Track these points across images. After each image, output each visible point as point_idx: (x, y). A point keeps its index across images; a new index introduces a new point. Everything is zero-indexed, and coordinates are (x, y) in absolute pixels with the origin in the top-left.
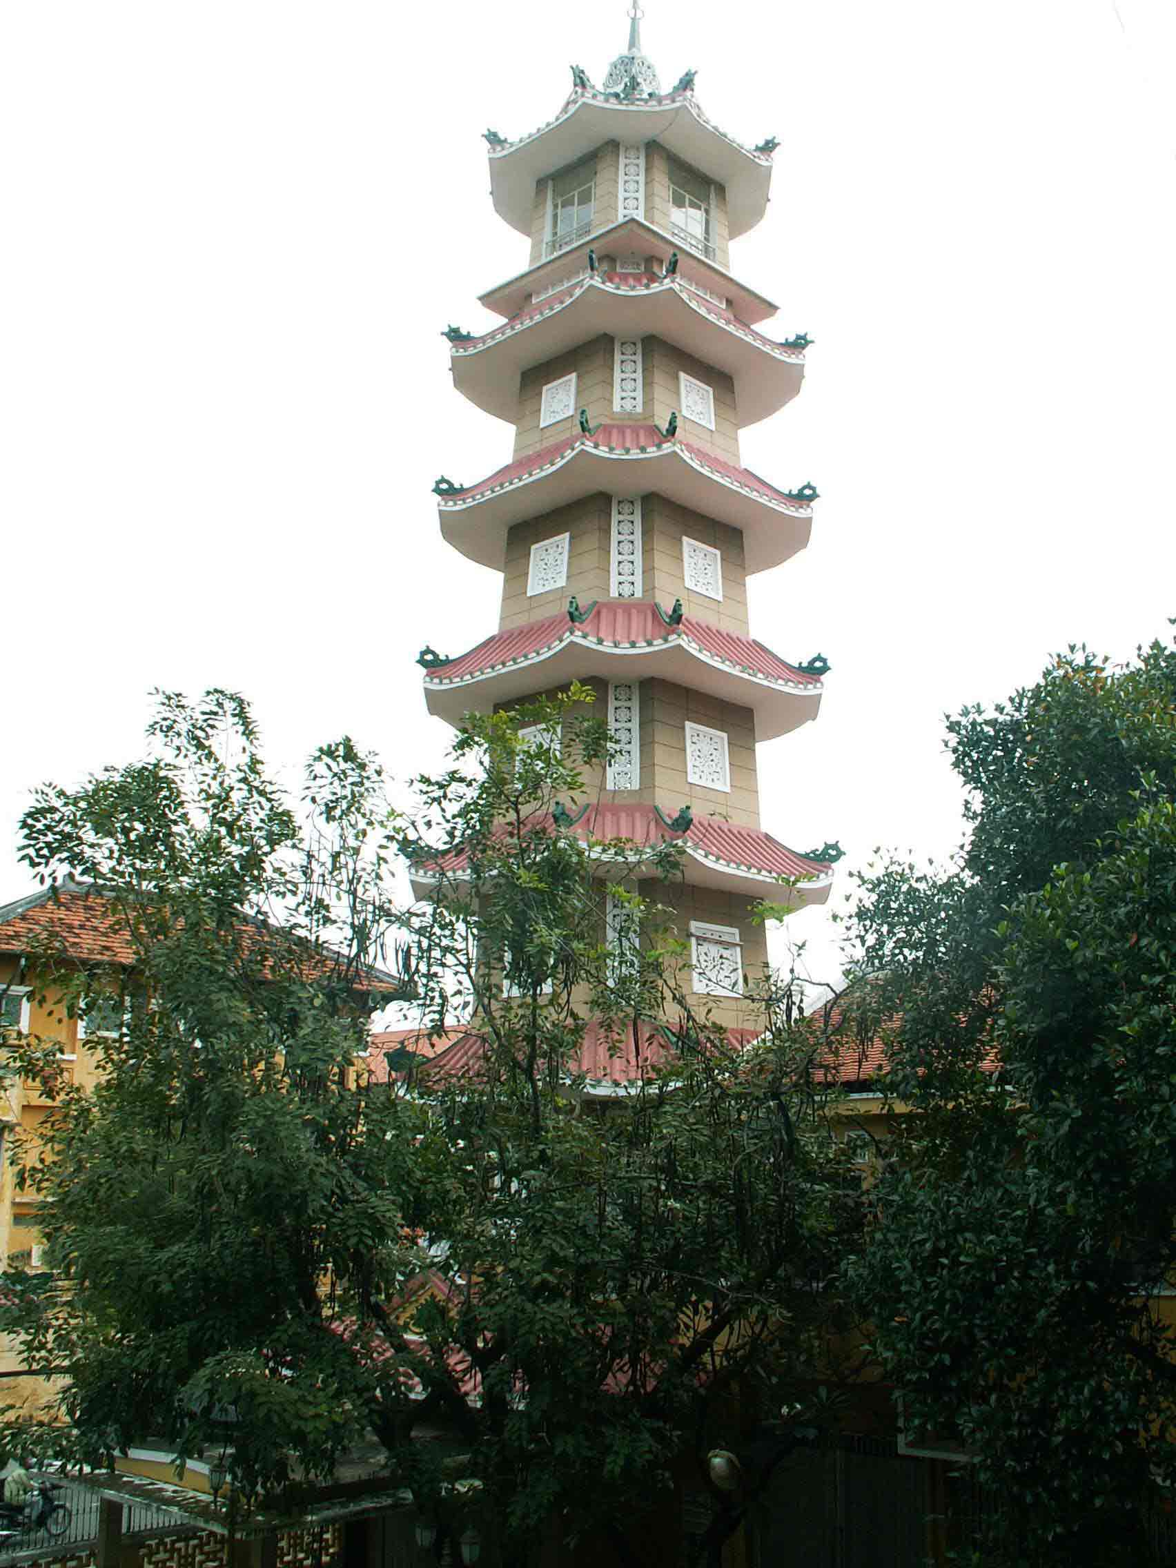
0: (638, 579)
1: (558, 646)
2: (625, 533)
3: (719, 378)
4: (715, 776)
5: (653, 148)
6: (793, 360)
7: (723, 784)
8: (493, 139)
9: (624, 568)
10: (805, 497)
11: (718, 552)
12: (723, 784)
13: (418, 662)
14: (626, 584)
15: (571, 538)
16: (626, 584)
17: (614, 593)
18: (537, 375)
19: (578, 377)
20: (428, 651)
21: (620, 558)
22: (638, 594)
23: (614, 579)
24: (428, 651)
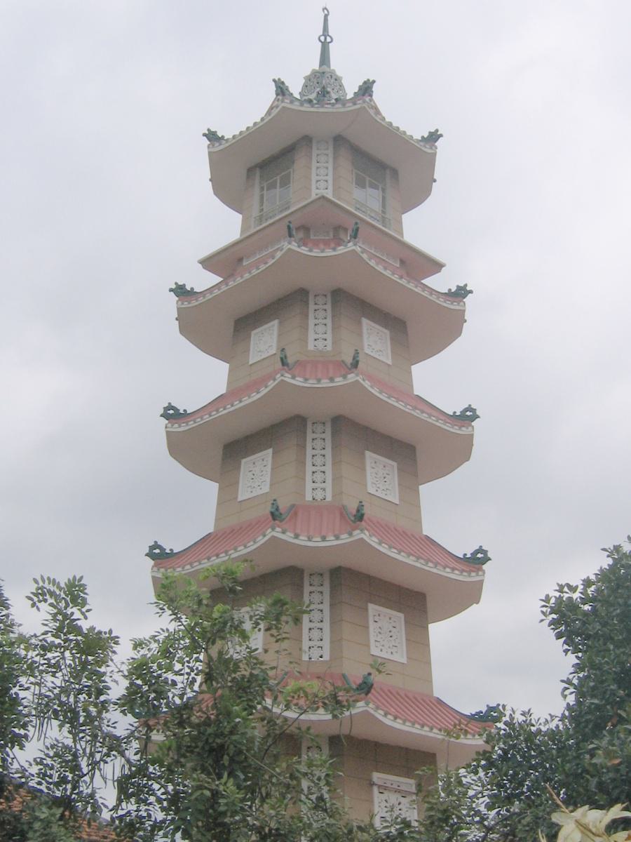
0: (329, 486)
1: (261, 540)
2: (319, 448)
3: (395, 323)
4: (394, 650)
5: (339, 141)
6: (455, 307)
7: (401, 657)
8: (212, 136)
9: (319, 334)
10: (468, 416)
11: (395, 464)
12: (401, 657)
13: (147, 555)
14: (319, 472)
15: (274, 453)
16: (319, 472)
17: (309, 498)
18: (247, 322)
19: (280, 323)
20: (156, 546)
21: (314, 469)
22: (329, 498)
23: (309, 486)
24: (170, 407)
